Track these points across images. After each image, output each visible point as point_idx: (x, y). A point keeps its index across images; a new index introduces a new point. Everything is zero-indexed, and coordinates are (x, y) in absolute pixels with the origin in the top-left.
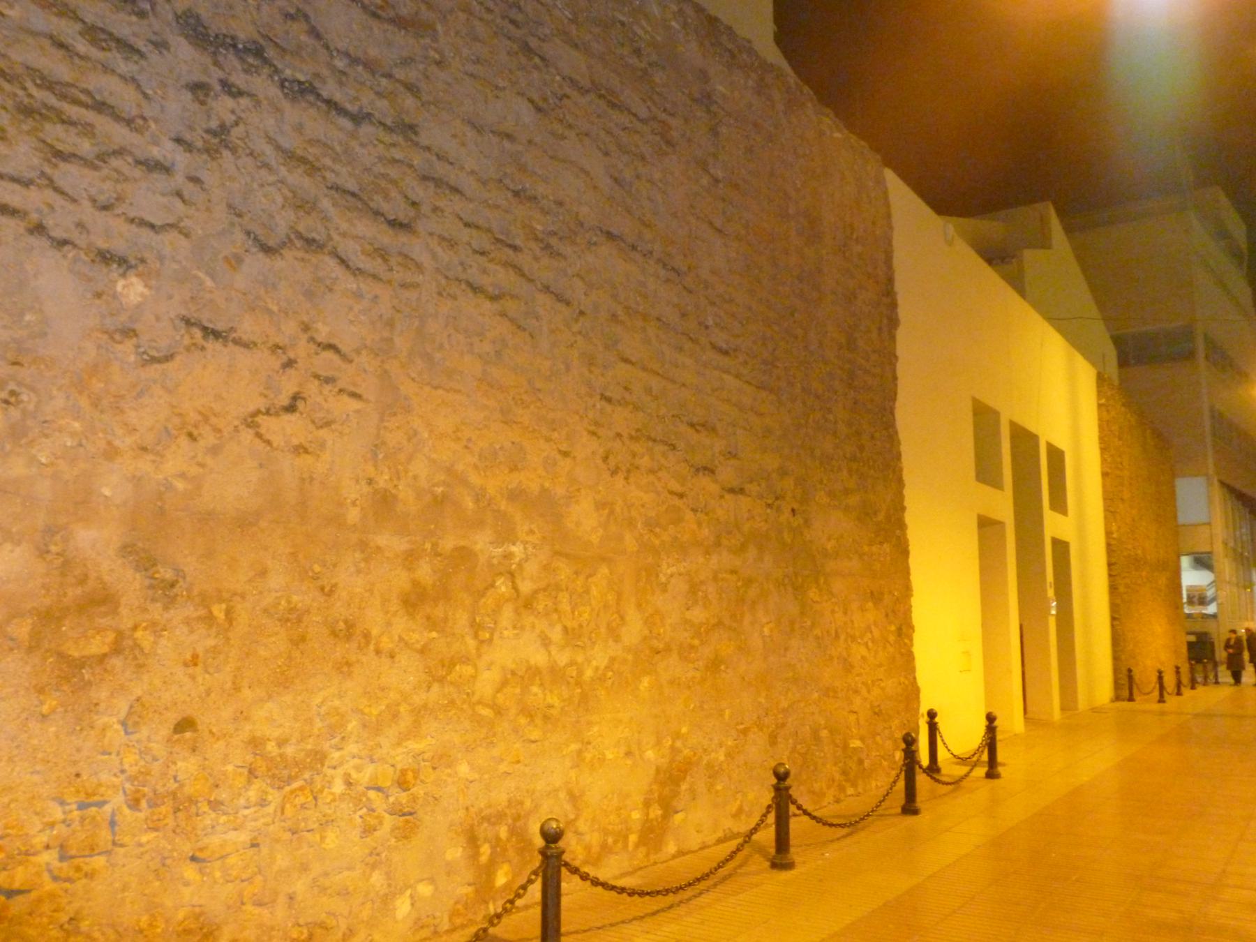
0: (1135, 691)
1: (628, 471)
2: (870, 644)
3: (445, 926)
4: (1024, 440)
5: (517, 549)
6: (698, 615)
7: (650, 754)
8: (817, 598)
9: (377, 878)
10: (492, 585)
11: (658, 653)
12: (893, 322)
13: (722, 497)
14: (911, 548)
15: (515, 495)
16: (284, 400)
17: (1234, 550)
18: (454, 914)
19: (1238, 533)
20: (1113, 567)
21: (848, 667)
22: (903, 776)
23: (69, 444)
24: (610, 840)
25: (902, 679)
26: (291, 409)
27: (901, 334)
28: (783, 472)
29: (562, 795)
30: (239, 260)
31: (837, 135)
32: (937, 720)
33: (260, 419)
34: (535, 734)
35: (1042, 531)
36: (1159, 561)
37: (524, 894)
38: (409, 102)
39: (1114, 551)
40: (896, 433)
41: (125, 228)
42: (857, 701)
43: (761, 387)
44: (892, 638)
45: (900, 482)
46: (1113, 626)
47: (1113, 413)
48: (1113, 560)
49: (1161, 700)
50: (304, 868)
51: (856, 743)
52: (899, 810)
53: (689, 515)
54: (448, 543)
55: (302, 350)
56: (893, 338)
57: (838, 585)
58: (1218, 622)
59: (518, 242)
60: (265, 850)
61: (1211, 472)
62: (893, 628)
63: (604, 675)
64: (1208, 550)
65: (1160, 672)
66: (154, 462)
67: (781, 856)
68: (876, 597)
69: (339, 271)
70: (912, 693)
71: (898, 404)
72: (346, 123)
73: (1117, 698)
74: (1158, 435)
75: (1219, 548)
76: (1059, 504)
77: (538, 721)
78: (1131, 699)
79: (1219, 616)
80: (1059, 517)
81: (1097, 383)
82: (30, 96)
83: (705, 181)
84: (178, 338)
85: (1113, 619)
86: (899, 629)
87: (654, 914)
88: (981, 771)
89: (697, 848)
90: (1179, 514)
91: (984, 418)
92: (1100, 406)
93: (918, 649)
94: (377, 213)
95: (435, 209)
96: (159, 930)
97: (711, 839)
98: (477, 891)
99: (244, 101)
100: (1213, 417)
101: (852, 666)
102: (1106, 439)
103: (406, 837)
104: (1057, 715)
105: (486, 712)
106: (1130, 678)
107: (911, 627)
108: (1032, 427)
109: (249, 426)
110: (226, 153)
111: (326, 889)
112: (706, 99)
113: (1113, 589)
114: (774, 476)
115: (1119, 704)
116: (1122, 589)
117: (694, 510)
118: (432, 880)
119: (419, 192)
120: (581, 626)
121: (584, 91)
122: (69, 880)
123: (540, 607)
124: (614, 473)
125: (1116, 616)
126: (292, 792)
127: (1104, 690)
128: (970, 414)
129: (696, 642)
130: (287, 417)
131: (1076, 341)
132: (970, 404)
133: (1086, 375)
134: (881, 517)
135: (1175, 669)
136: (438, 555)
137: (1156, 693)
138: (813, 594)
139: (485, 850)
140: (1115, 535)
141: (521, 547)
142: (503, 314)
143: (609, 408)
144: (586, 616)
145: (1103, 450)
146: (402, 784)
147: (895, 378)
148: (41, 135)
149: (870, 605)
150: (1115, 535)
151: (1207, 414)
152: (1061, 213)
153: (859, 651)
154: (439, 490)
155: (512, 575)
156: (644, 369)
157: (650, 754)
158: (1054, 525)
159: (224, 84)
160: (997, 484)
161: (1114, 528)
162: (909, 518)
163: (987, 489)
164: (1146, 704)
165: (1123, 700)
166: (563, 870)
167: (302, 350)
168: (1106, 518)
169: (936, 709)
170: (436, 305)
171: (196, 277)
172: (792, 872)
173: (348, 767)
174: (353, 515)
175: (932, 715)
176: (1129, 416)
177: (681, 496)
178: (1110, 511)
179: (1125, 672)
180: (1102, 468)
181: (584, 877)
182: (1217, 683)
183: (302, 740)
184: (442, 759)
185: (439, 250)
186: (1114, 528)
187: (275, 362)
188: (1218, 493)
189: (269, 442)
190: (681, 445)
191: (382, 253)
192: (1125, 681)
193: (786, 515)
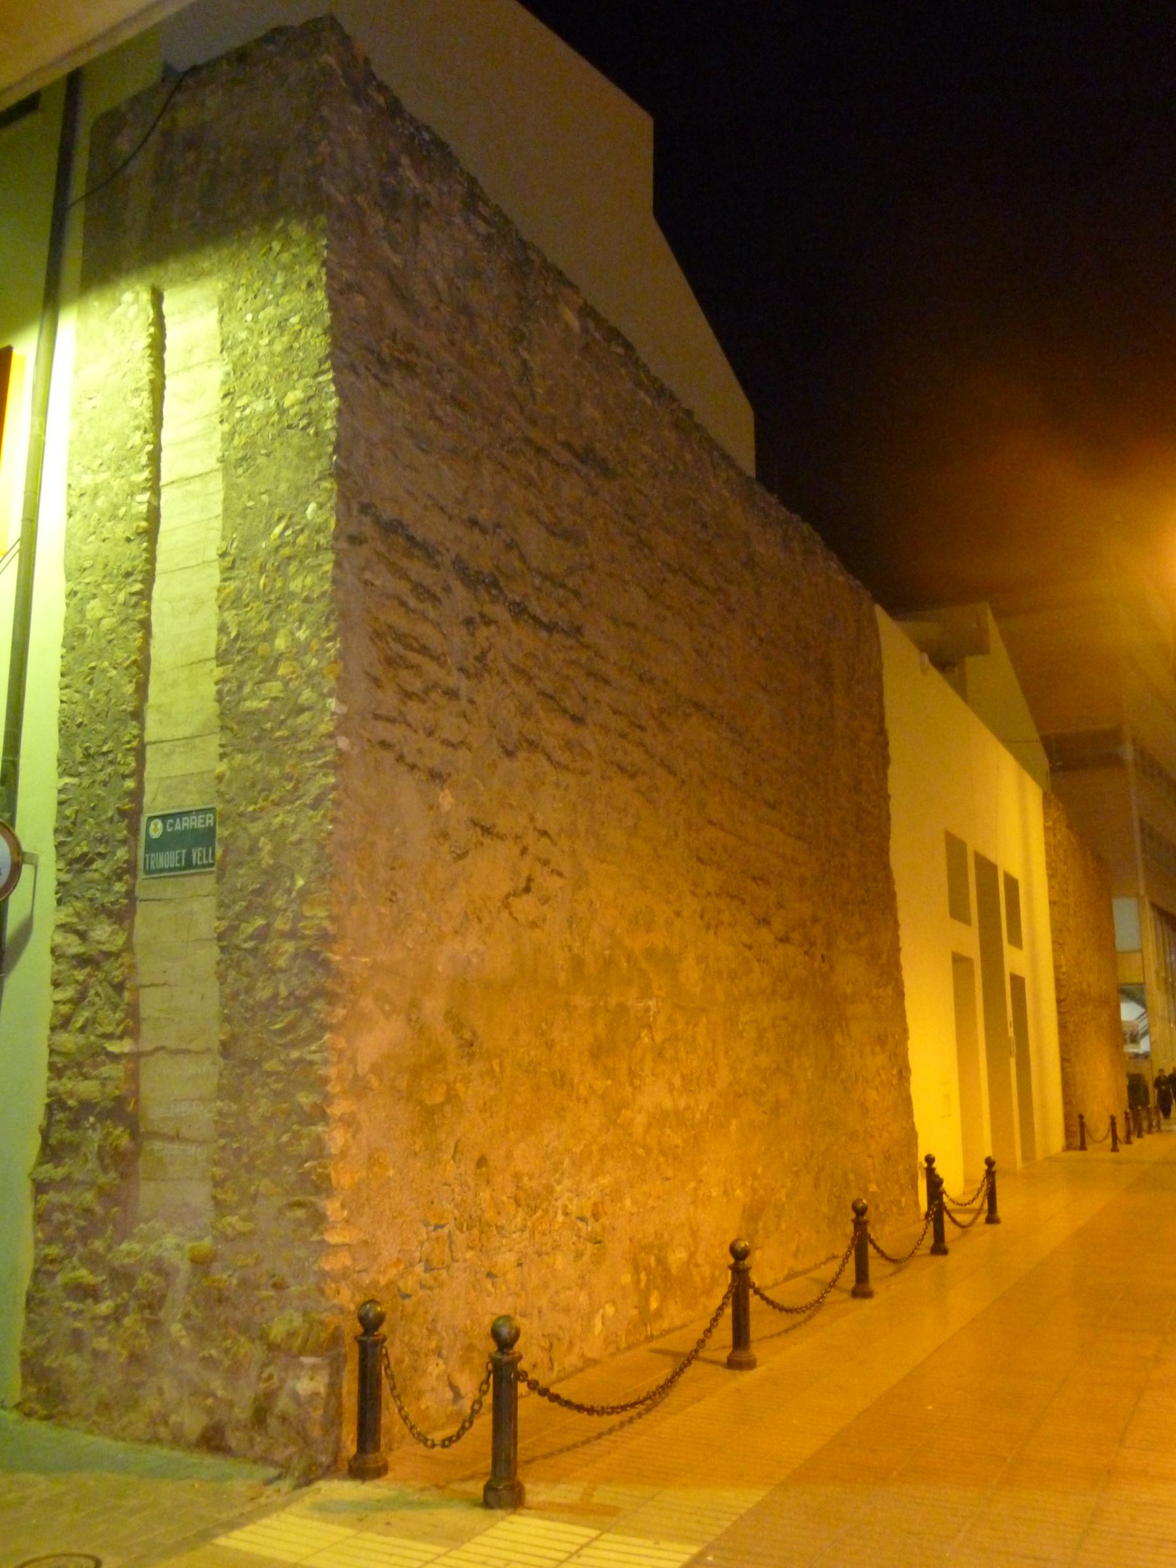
0: (1087, 1139)
1: (716, 927)
2: (879, 1088)
3: (623, 1345)
4: (987, 869)
5: (652, 1003)
6: (764, 1060)
7: (738, 1192)
8: (841, 1043)
9: (583, 1298)
10: (639, 1037)
11: (740, 1096)
12: (886, 760)
13: (776, 946)
14: (906, 990)
15: (650, 953)
16: (522, 884)
17: (1166, 980)
18: (629, 1333)
19: (1168, 960)
20: (1062, 1004)
21: (864, 1110)
23: (421, 931)
24: (717, 1273)
25: (904, 1124)
26: (527, 890)
27: (892, 771)
28: (815, 920)
29: (686, 1230)
30: (494, 765)
31: (841, 579)
33: (511, 899)
34: (670, 1173)
35: (1003, 967)
36: (1101, 996)
38: (575, 606)
39: (1064, 986)
40: (891, 872)
41: (440, 749)
43: (799, 837)
44: (895, 1081)
45: (896, 924)
46: (1063, 1069)
47: (1059, 837)
48: (1062, 996)
49: (1115, 1149)
50: (546, 1286)
51: (873, 1188)
53: (756, 966)
54: (613, 1001)
55: (530, 838)
56: (885, 778)
57: (855, 1029)
58: (1151, 1061)
59: (643, 723)
60: (525, 1268)
61: (1142, 892)
62: (895, 1072)
63: (708, 1118)
66: (461, 941)
67: (862, 1290)
68: (881, 1040)
69: (547, 767)
70: (911, 1137)
71: (892, 843)
72: (544, 634)
73: (1068, 1147)
74: (1098, 858)
75: (1152, 980)
76: (1016, 940)
77: (670, 1160)
78: (1083, 1147)
79: (1154, 1057)
80: (1015, 950)
81: (1044, 803)
82: (391, 649)
83: (754, 642)
84: (469, 837)
86: (900, 1072)
87: (786, 1331)
88: (983, 1217)
89: (770, 1284)
90: (1117, 942)
91: (955, 847)
92: (1046, 829)
94: (565, 711)
95: (597, 701)
96: (476, 1333)
97: (780, 1277)
98: (640, 1313)
99: (493, 628)
100: (1142, 830)
101: (867, 1111)
102: (1054, 865)
103: (599, 1263)
104: (1020, 1165)
105: (640, 1151)
106: (1082, 1125)
107: (909, 1070)
108: (992, 857)
109: (506, 907)
110: (486, 675)
111: (556, 1305)
112: (750, 563)
113: (1063, 1027)
114: (809, 923)
115: (1071, 1153)
116: (1071, 1027)
117: (759, 961)
118: (613, 1302)
119: (588, 687)
120: (692, 1073)
121: (675, 572)
122: (431, 1288)
123: (668, 1056)
124: (708, 927)
125: (1067, 1057)
126: (538, 1219)
127: (1056, 1139)
128: (943, 844)
129: (764, 1086)
130: (525, 897)
131: (1024, 762)
132: (942, 836)
133: (1034, 794)
134: (884, 957)
135: (1124, 1116)
136: (608, 1011)
137: (1109, 1141)
138: (838, 1038)
139: (643, 1276)
140: (1064, 969)
141: (655, 1002)
142: (638, 790)
143: (702, 867)
144: (695, 1063)
145: (1051, 877)
146: (596, 1216)
147: (889, 818)
148: (397, 680)
149: (878, 1049)
150: (1064, 969)
151: (1136, 824)
152: (998, 615)
153: (873, 1095)
154: (607, 952)
155: (650, 1026)
156: (722, 828)
157: (738, 1192)
158: (1014, 960)
159: (482, 616)
160: (966, 920)
161: (1063, 962)
162: (905, 959)
163: (957, 924)
164: (1099, 1151)
165: (1075, 1149)
167: (530, 838)
168: (1054, 950)
171: (474, 784)
172: (752, 1373)
173: (564, 1200)
174: (562, 978)
175: (930, 1160)
176: (1072, 838)
177: (750, 947)
178: (1058, 944)
179: (1076, 1115)
180: (1050, 895)
182: (1159, 1130)
183: (540, 1175)
184: (616, 1195)
185: (599, 737)
186: (1063, 962)
187: (517, 851)
188: (1149, 913)
189: (516, 919)
190: (748, 900)
191: (568, 745)
192: (1076, 1128)
193: (817, 963)
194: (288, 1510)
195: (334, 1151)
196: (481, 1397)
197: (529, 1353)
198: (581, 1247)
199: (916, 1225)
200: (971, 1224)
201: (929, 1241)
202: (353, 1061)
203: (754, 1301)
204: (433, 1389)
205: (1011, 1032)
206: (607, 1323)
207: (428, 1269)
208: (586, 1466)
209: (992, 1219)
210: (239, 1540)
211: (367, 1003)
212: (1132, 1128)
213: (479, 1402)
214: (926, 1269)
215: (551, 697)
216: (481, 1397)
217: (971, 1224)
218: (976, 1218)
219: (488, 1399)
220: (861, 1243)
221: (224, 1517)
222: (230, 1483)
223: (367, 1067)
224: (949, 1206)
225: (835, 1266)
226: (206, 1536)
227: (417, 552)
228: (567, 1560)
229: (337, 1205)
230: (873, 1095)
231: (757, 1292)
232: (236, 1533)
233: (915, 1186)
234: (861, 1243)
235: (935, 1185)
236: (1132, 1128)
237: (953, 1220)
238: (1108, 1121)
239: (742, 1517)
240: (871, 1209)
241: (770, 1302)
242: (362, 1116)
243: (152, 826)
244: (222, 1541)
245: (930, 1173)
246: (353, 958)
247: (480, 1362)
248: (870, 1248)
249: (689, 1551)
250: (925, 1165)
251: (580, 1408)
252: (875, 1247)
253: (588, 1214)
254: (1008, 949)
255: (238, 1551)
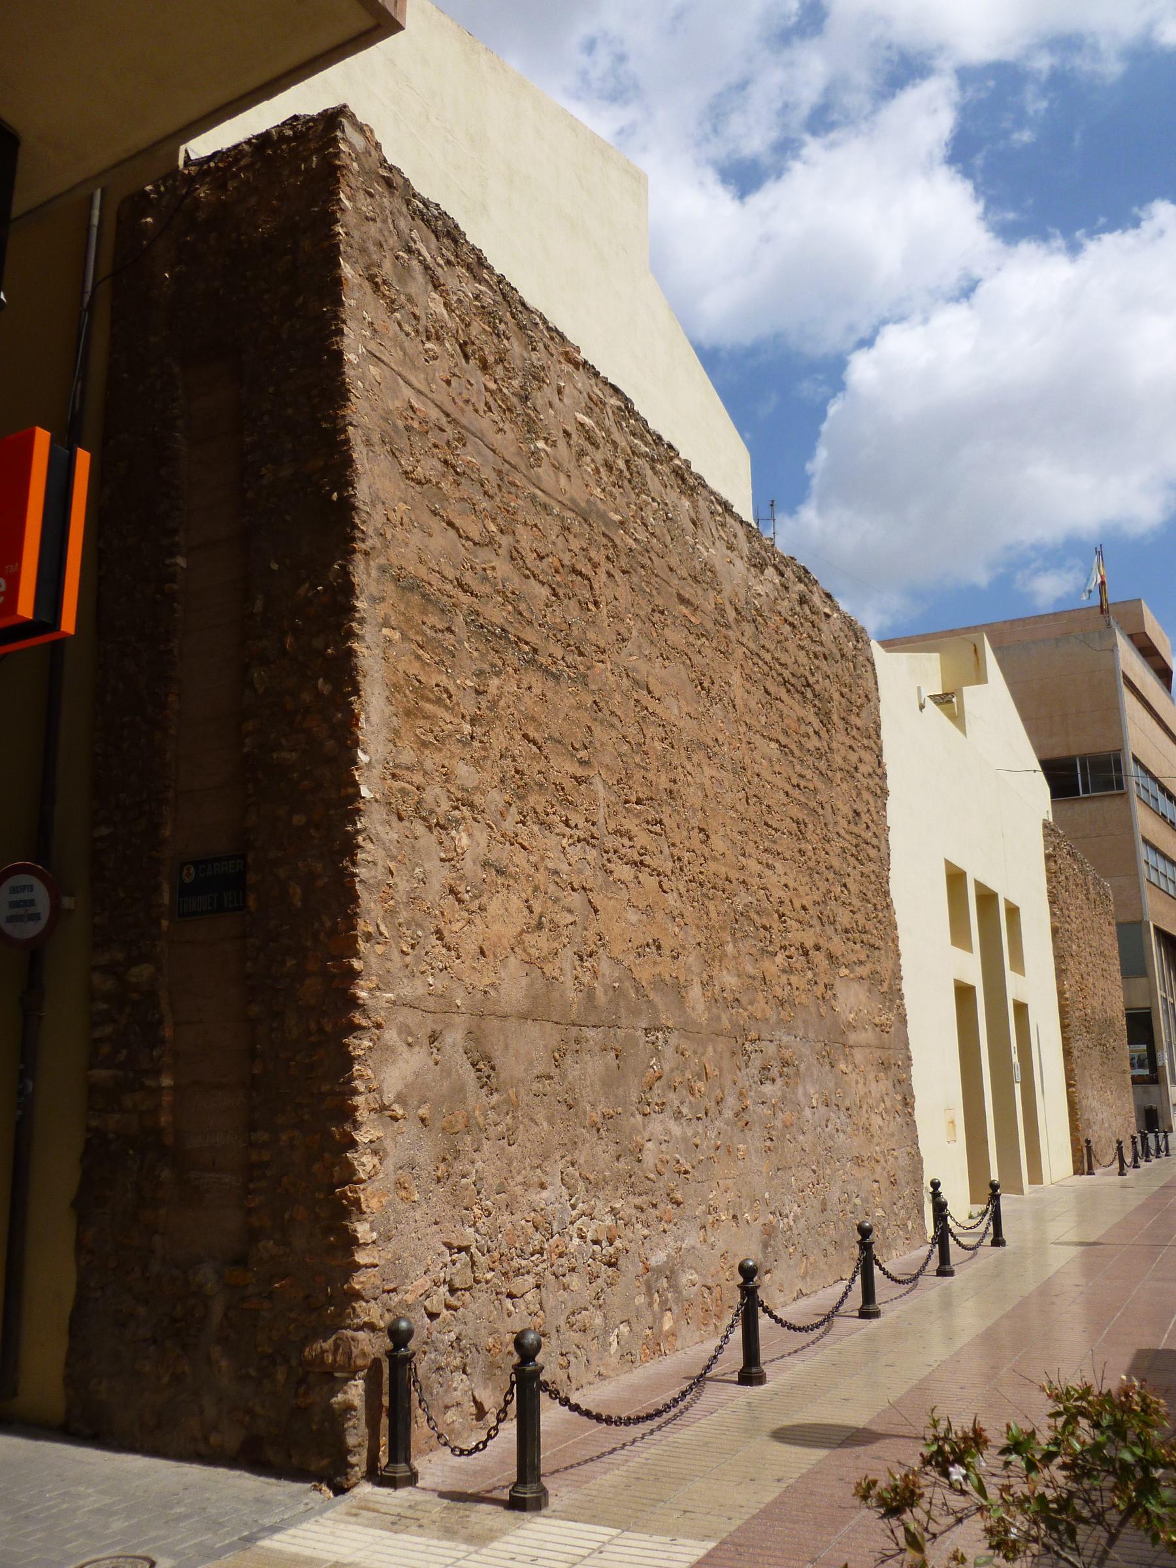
4: (987, 899)
22: (859, 1278)
26: (540, 926)
32: (940, 1189)
37: (455, 1455)
42: (878, 1169)
44: (899, 1107)
52: (857, 1314)
62: (899, 1098)
64: (1148, 1006)
65: (1119, 1143)
73: (1078, 1171)
78: (1090, 1172)
85: (1069, 1086)
88: (988, 1240)
93: (918, 1116)
106: (1089, 1148)
113: (1067, 1053)
137: (1117, 1165)
153: (877, 1121)
158: (1015, 987)
160: (968, 947)
166: (544, 1397)
169: (939, 1178)
170: (675, 782)
172: (762, 1387)
175: (935, 1185)
181: (565, 1402)
194: (326, 1515)
195: (363, 1176)
196: (497, 1424)
197: (549, 1364)
198: (595, 1268)
199: (922, 1251)
200: (979, 1244)
201: (934, 1263)
202: (381, 1093)
203: (764, 1320)
204: (458, 1404)
205: (1015, 1058)
206: (622, 1343)
207: (453, 1291)
208: (605, 1473)
209: (998, 1241)
210: (277, 1543)
211: (391, 1035)
212: (1140, 1153)
213: (504, 1411)
214: (932, 1285)
215: (560, 742)
216: (497, 1424)
217: (979, 1244)
218: (981, 1240)
219: (513, 1408)
220: (867, 1264)
221: (267, 1521)
222: (822, 454)
223: (392, 1096)
224: (956, 1230)
225: (841, 1288)
226: (251, 1539)
227: (430, 608)
228: (589, 1555)
229: (367, 1226)
230: (877, 1121)
231: (766, 1310)
232: (278, 1536)
233: (921, 1211)
234: (867, 1264)
235: (940, 1209)
236: (1140, 1153)
237: (958, 1242)
238: (1115, 1145)
239: (754, 1517)
240: (875, 1232)
241: (778, 1320)
242: (388, 1144)
243: (185, 871)
244: (266, 1543)
245: (936, 1195)
246: (378, 994)
247: (505, 1378)
248: (876, 1269)
249: (699, 1549)
250: (931, 1190)
251: (598, 1418)
252: (881, 1268)
253: (603, 1238)
254: (1010, 976)
255: (281, 1552)
